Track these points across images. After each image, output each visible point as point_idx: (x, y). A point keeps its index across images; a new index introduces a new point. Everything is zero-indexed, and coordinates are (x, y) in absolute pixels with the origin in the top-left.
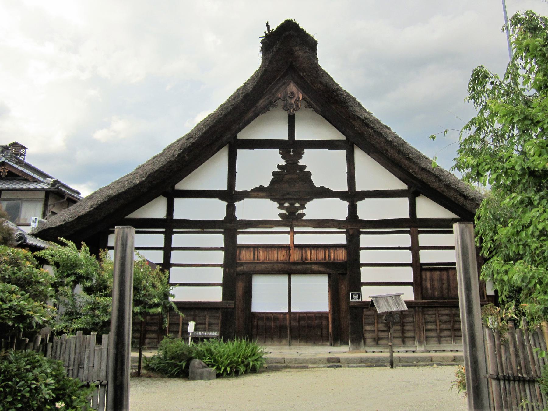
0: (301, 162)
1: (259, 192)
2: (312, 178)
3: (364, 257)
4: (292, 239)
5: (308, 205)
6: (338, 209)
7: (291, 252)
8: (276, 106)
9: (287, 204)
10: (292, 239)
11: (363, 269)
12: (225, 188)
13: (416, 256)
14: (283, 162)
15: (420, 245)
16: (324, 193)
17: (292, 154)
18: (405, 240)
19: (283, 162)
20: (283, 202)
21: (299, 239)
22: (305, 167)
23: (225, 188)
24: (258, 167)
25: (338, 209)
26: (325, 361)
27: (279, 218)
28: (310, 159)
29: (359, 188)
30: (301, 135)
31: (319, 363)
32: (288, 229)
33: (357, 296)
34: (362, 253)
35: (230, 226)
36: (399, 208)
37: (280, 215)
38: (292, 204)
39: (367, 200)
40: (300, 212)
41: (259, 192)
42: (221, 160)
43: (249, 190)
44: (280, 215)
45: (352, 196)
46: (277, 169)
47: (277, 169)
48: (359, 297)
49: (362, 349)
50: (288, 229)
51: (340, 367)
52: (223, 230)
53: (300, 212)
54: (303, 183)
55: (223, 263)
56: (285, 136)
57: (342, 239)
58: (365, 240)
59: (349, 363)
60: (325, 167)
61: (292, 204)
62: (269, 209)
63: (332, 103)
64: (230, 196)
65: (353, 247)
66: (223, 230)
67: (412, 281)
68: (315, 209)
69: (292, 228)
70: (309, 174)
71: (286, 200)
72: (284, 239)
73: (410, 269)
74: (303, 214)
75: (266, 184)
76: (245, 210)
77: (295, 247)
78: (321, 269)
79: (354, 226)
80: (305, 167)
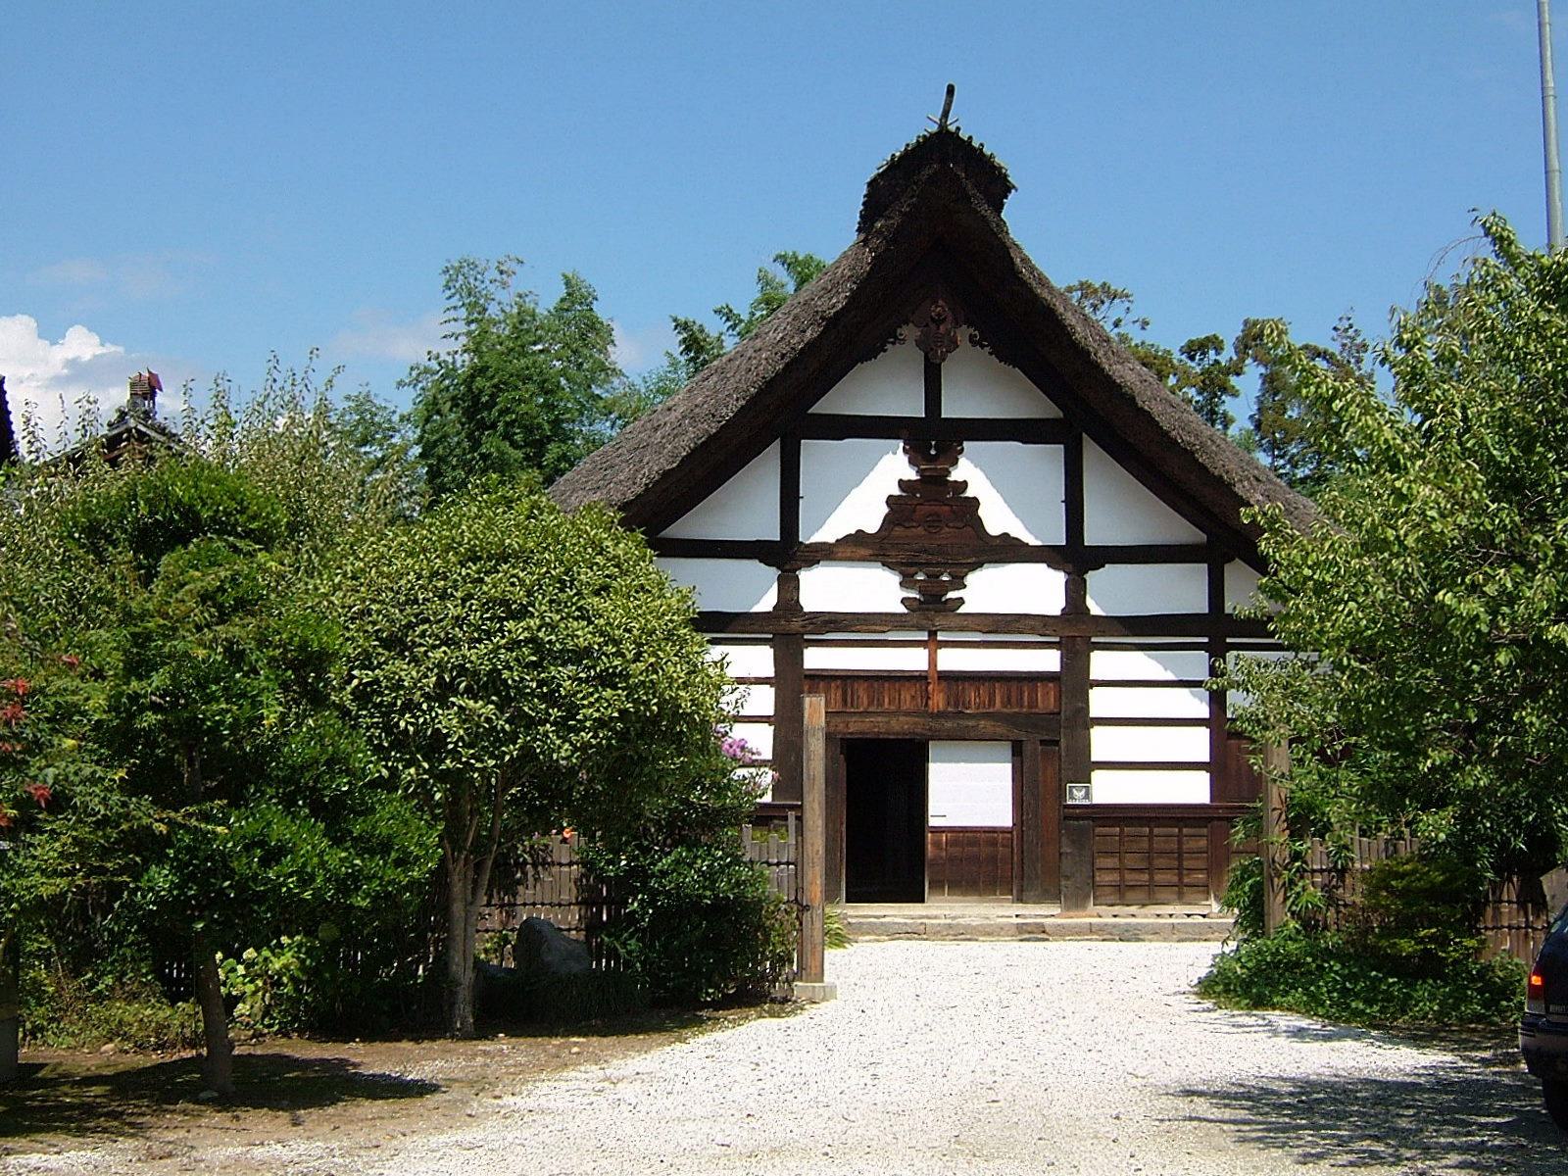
0: (956, 475)
1: (856, 548)
2: (981, 512)
3: (1100, 703)
4: (933, 661)
5: (971, 579)
6: (1039, 590)
7: (930, 687)
8: (896, 340)
9: (920, 577)
10: (933, 661)
11: (1096, 732)
12: (775, 535)
13: (1217, 699)
14: (911, 474)
15: (1094, 758)
16: (1009, 550)
17: (933, 452)
18: (1196, 664)
19: (911, 474)
20: (912, 570)
21: (951, 660)
22: (965, 484)
23: (775, 535)
24: (863, 488)
25: (1039, 590)
26: (1014, 930)
27: (902, 609)
28: (969, 471)
29: (1091, 538)
30: (953, 407)
31: (999, 935)
32: (924, 636)
33: (1083, 792)
34: (1095, 694)
35: (789, 629)
36: (1181, 590)
37: (904, 601)
38: (933, 577)
39: (1109, 569)
40: (952, 595)
41: (856, 548)
42: (766, 469)
43: (832, 540)
44: (904, 601)
45: (1075, 558)
46: (896, 492)
47: (896, 492)
48: (1087, 795)
49: (1091, 907)
50: (924, 636)
51: (1047, 940)
52: (1206, 640)
53: (952, 595)
54: (960, 525)
55: (772, 713)
56: (916, 409)
57: (1048, 661)
58: (1103, 664)
59: (1063, 933)
60: (1003, 490)
61: (933, 577)
62: (877, 589)
63: (1033, 333)
64: (787, 555)
65: (1074, 681)
66: (1206, 640)
67: (1207, 759)
68: (989, 590)
69: (933, 634)
70: (975, 503)
71: (920, 566)
72: (913, 660)
73: (1204, 733)
74: (961, 601)
75: (872, 525)
76: (825, 589)
77: (939, 678)
78: (1001, 730)
79: (1075, 632)
80: (965, 484)
